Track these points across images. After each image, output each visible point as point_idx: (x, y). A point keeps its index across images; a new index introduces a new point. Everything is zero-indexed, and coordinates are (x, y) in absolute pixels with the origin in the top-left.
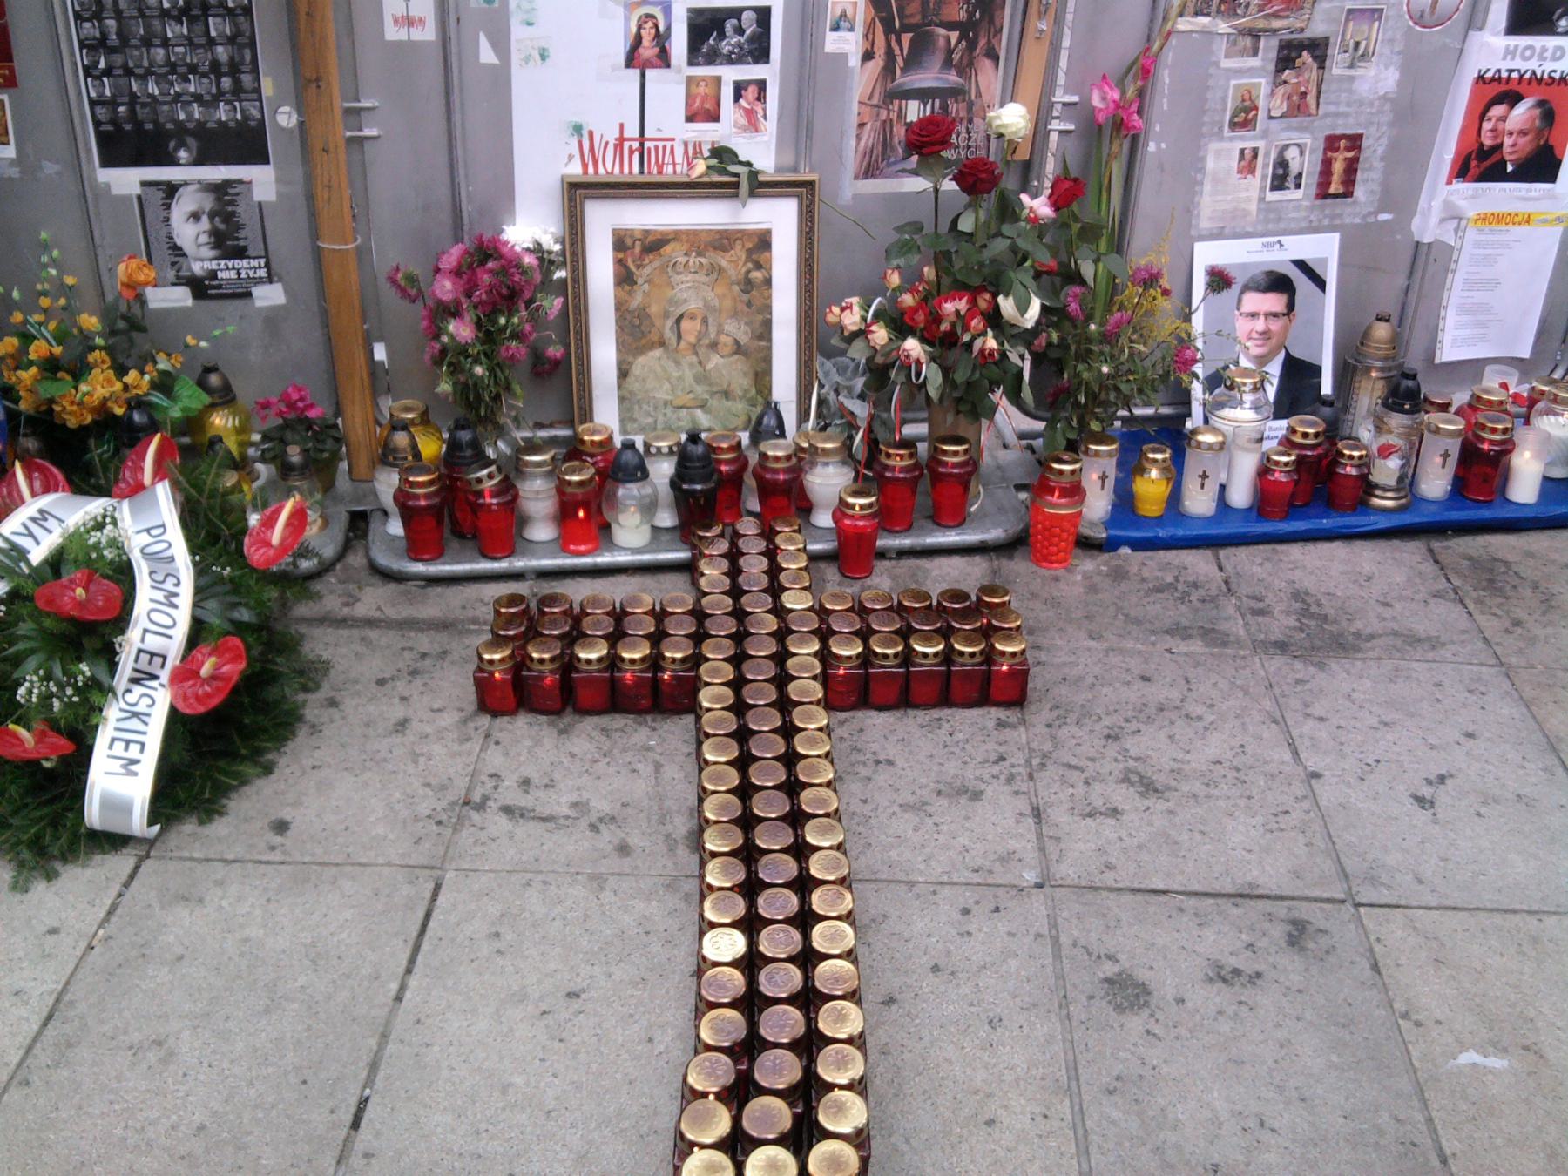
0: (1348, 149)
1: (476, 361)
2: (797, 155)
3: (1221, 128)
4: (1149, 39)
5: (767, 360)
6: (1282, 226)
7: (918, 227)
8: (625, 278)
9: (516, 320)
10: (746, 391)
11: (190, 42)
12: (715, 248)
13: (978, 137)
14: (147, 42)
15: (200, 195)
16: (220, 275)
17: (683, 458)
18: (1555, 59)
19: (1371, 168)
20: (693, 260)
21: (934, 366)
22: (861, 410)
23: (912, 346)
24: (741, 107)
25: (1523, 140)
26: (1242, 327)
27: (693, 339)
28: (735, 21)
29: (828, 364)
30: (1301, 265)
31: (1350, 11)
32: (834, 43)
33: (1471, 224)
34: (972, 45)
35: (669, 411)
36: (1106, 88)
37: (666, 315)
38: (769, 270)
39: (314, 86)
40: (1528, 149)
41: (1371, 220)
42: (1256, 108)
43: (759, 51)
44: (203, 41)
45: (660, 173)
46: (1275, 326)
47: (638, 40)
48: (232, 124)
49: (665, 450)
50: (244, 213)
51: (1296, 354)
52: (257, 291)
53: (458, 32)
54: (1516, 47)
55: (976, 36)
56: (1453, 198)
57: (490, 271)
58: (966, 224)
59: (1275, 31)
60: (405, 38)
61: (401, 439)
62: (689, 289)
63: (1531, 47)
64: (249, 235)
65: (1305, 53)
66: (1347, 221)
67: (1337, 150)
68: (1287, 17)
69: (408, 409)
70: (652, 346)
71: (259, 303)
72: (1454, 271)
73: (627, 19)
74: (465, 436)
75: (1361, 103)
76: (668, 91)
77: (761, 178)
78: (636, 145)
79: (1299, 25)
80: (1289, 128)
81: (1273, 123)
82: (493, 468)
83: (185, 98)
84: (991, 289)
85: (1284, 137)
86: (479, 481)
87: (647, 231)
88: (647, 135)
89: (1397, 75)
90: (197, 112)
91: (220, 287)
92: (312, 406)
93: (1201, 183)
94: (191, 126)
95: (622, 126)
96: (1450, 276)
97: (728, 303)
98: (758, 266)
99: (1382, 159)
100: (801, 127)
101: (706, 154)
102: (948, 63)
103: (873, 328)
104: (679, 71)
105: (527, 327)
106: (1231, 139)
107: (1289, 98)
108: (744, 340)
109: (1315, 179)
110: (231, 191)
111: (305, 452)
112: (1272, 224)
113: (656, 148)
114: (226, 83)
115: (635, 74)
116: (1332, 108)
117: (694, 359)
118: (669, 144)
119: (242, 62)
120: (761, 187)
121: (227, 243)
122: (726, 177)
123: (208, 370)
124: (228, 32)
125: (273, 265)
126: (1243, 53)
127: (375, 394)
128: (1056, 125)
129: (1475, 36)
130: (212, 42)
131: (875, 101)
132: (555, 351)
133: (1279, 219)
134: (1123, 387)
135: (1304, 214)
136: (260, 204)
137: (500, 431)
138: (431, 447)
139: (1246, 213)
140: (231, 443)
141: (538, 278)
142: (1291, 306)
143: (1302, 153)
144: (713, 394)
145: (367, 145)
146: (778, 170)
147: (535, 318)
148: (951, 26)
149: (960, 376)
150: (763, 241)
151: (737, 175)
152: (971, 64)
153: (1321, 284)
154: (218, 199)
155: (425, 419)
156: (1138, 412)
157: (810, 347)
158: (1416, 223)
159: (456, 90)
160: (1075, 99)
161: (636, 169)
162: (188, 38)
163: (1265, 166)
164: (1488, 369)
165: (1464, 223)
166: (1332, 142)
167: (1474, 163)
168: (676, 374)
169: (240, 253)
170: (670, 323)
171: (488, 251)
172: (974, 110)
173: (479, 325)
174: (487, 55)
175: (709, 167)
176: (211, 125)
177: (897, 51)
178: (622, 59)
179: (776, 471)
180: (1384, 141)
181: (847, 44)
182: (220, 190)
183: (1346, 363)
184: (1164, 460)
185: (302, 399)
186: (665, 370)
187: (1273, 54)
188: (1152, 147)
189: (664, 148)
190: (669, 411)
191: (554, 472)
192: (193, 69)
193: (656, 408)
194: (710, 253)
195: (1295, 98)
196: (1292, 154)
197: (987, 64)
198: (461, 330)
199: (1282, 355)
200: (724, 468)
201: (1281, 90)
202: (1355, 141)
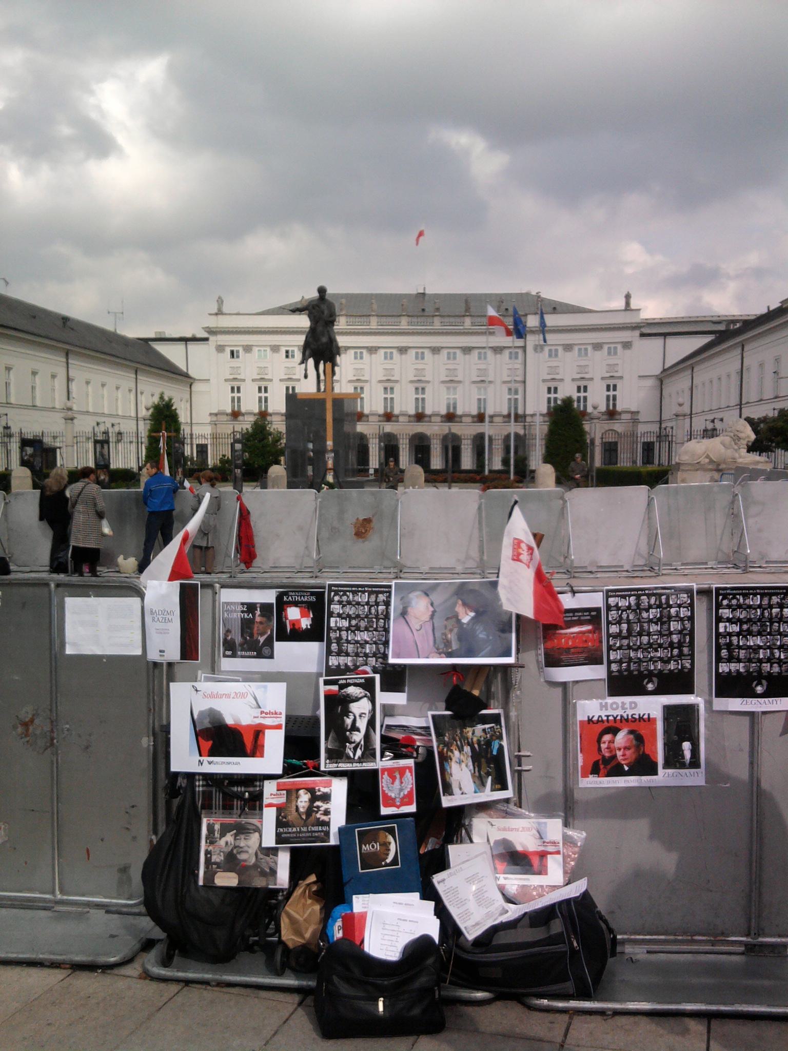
11: (660, 634)
14: (640, 634)
18: (631, 708)
25: (628, 753)
40: (634, 757)
63: (615, 703)
90: (659, 665)
119: (685, 642)
130: (671, 633)
162: (660, 632)
167: (602, 767)
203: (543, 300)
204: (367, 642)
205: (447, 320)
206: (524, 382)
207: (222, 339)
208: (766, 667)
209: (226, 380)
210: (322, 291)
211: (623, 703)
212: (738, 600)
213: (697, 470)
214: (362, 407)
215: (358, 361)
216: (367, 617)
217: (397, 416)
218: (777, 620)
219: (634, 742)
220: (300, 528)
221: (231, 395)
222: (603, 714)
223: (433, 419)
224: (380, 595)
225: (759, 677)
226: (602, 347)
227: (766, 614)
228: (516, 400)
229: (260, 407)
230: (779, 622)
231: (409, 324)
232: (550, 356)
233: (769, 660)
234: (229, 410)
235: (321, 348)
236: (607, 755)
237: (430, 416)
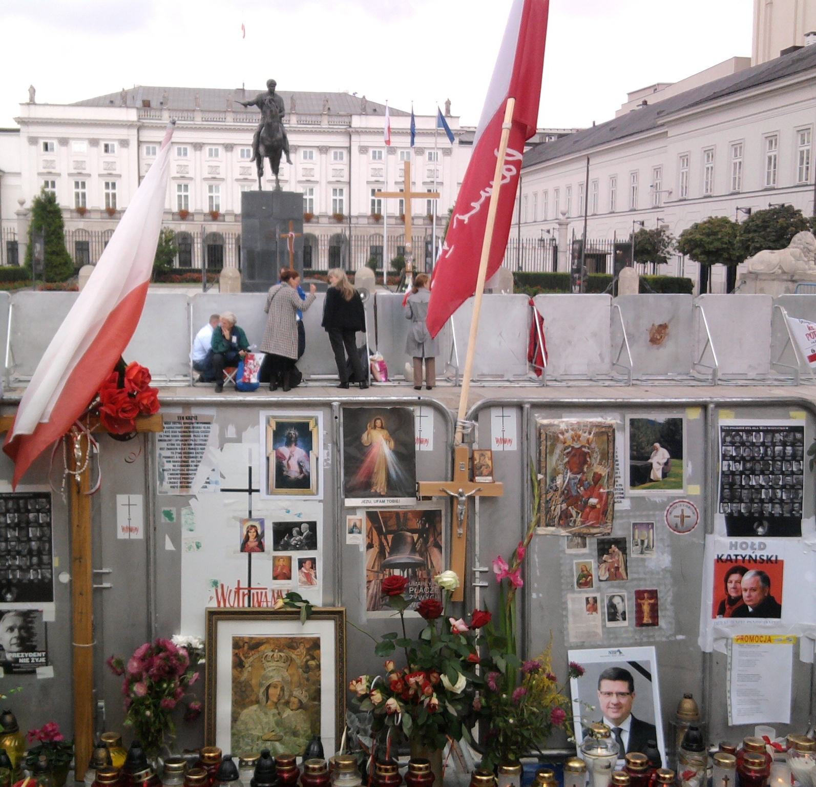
0: (651, 599)
1: (148, 708)
2: (334, 597)
3: (572, 586)
4: (523, 538)
5: (318, 713)
6: (619, 642)
7: (395, 635)
8: (238, 664)
9: (173, 685)
10: (306, 731)
11: (18, 540)
12: (289, 648)
13: (435, 589)
15: (15, 618)
16: (20, 661)
17: (259, 767)
18: (761, 549)
19: (666, 609)
20: (277, 654)
21: (407, 715)
22: (367, 741)
23: (392, 703)
24: (302, 572)
25: (754, 594)
26: (603, 700)
27: (275, 700)
28: (298, 529)
29: (354, 716)
30: (634, 664)
31: (634, 524)
32: (350, 539)
33: (734, 642)
34: (426, 541)
35: (260, 742)
36: (500, 563)
37: (261, 685)
38: (319, 660)
39: (78, 561)
41: (673, 639)
42: (591, 575)
43: (311, 543)
44: (25, 539)
45: (259, 606)
46: (624, 700)
47: (247, 538)
48: (36, 581)
49: (250, 764)
50: (37, 628)
51: (640, 717)
52: (39, 670)
53: (155, 535)
54: (736, 543)
55: (427, 536)
56: (720, 627)
57: (161, 658)
58: (426, 636)
59: (593, 535)
60: (127, 537)
61: (102, 753)
62: (274, 672)
64: (38, 640)
65: (613, 546)
66: (658, 639)
67: (643, 599)
68: (599, 527)
69: (110, 738)
70: (252, 703)
71: (39, 677)
72: (730, 670)
73: (241, 528)
74: (137, 752)
75: (652, 573)
76: (263, 563)
77: (313, 609)
78: (246, 591)
79: (607, 531)
80: (612, 586)
81: (603, 584)
82: (148, 770)
83: (14, 568)
84: (438, 671)
85: (611, 591)
86: (140, 777)
87: (252, 638)
88: (252, 586)
89: (670, 558)
90: (18, 574)
91: (19, 667)
92: (57, 734)
93: (566, 616)
94: (15, 581)
95: (239, 582)
96: (728, 673)
97: (296, 679)
98: (313, 658)
99: (671, 604)
100: (337, 581)
101: (284, 596)
102: (414, 550)
103: (373, 693)
104: (269, 553)
105: (179, 690)
106: (580, 592)
107: (609, 570)
108: (305, 700)
109: (634, 615)
110: (32, 615)
111: (49, 761)
112: (612, 641)
113: (257, 593)
114: (35, 560)
115: (246, 555)
116: (636, 576)
117: (276, 711)
118: (264, 591)
119: (44, 549)
120: (313, 614)
121: (26, 644)
122: (294, 608)
123: (6, 713)
124: (38, 535)
125: (50, 655)
126: (577, 546)
127: (95, 731)
128: (478, 583)
129: (709, 537)
130: (30, 540)
131: (376, 569)
132: (195, 705)
133: (616, 638)
134: (526, 734)
135: (631, 635)
136: (46, 623)
137: (161, 752)
138: (118, 760)
139: (596, 634)
140: (12, 757)
141: (188, 662)
142: (631, 688)
143: (623, 600)
144: (285, 733)
145: (105, 593)
146: (324, 605)
147: (184, 685)
148: (413, 531)
149: (420, 722)
150: (315, 644)
151: (300, 607)
152: (426, 550)
153: (648, 676)
154: (25, 620)
155: (119, 744)
156: (545, 752)
157: (342, 705)
158: (700, 641)
159: (152, 564)
160: (486, 569)
161: (246, 604)
163: (603, 607)
164: (756, 728)
165: (730, 641)
166: (640, 595)
167: (727, 607)
168: (265, 720)
169: (33, 649)
170: (262, 690)
171: (162, 648)
172: (430, 576)
173: (150, 688)
174: (169, 546)
175: (285, 603)
176: (25, 581)
177: (385, 544)
178: (239, 548)
179: (315, 777)
180: (671, 593)
181: (358, 540)
182: (26, 616)
183: (670, 724)
184: (549, 778)
185: (53, 730)
186: (259, 717)
187: (595, 546)
188: (534, 596)
189: (262, 593)
190: (260, 742)
191: (184, 776)
192: (19, 553)
193: (252, 741)
194: (286, 651)
195: (612, 570)
196: (617, 601)
197: (435, 550)
198: (139, 689)
199: (629, 719)
200: (286, 775)
201: (604, 566)
202: (653, 594)
203: (367, 101)
204: (762, 487)
205: (303, 118)
206: (350, 183)
207: (35, 131)
208: (768, 507)
209: (39, 174)
210: (272, 84)
211: (752, 543)
212: (742, 437)
213: (774, 280)
214: (311, 208)
215: (213, 158)
216: (762, 458)
217: (224, 216)
218: (779, 458)
219: (760, 583)
220: (594, 335)
221: (188, 194)
222: (732, 553)
223: (93, 215)
224: (777, 435)
225: (760, 519)
226: (367, 151)
227: (769, 452)
228: (341, 201)
229: (77, 203)
230: (781, 461)
231: (235, 120)
232: (374, 157)
233: (771, 501)
234: (331, 213)
235: (271, 147)
236: (733, 595)
237: (318, 217)
